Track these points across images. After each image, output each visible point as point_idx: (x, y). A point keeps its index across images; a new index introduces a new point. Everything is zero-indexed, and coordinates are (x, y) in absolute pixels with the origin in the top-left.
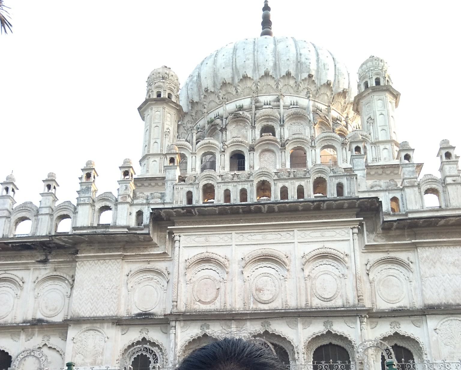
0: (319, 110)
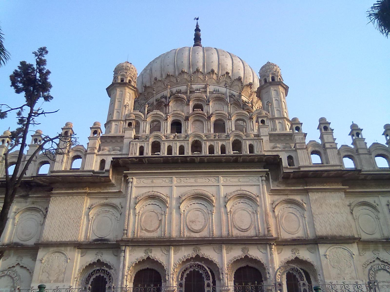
0: (233, 95)
